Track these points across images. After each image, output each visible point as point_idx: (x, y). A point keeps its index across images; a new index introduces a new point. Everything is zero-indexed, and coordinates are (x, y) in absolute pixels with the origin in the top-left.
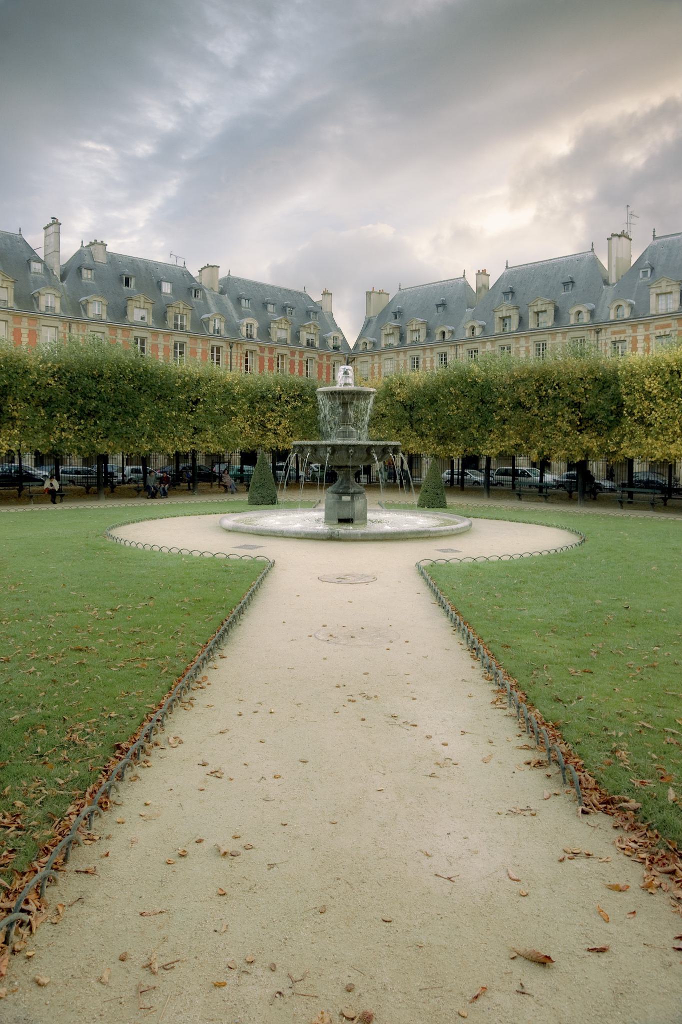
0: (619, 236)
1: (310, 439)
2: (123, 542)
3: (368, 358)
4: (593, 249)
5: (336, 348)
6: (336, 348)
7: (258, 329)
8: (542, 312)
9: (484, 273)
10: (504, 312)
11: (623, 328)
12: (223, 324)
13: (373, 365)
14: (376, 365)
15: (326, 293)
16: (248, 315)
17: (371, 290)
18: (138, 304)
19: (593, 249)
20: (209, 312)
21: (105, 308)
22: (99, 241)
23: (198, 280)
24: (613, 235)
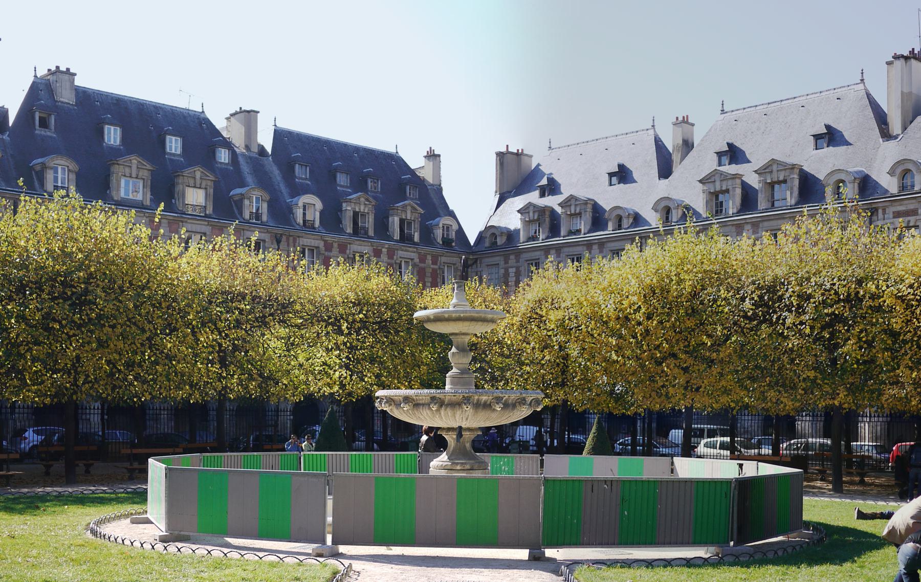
0: (906, 58)
1: (519, 480)
2: (137, 544)
3: (499, 260)
4: (862, 80)
5: (447, 242)
6: (447, 242)
7: (322, 213)
8: (779, 182)
9: (685, 121)
10: (718, 184)
11: (911, 207)
12: (265, 205)
13: (506, 270)
14: (512, 271)
15: (432, 156)
16: (305, 191)
17: (504, 150)
18: (127, 170)
19: (862, 80)
20: (243, 184)
21: (73, 177)
22: (63, 68)
23: (225, 134)
24: (896, 57)
